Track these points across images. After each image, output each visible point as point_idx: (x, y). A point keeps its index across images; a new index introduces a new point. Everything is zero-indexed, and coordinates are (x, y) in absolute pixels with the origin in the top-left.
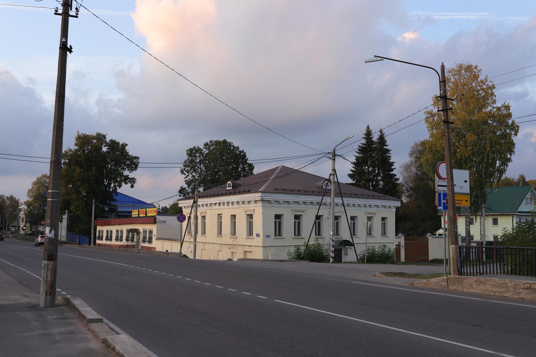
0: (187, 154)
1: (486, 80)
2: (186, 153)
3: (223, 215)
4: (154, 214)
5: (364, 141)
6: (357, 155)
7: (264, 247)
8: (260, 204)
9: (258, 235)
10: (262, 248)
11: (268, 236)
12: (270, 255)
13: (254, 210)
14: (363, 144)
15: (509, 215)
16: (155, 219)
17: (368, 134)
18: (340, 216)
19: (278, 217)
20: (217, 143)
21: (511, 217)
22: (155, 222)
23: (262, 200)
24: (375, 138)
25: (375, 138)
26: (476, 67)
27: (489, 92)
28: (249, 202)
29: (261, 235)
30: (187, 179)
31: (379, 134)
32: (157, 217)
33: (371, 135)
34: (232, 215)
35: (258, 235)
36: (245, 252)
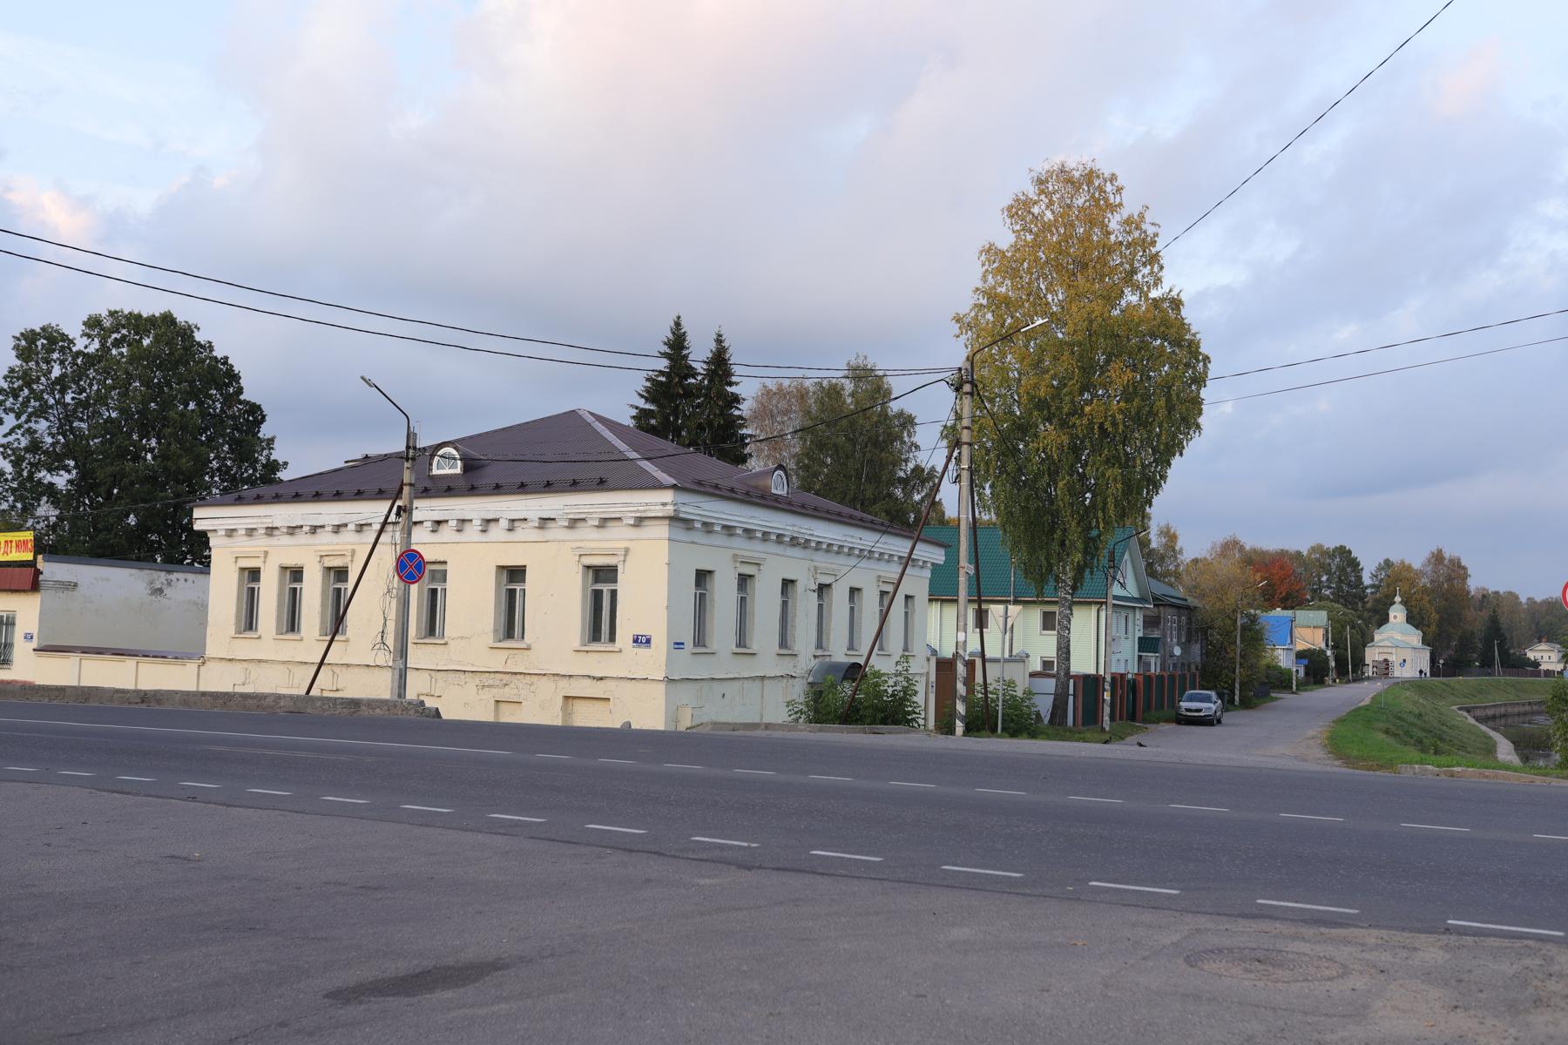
0: (16, 347)
1: (1142, 216)
2: (12, 343)
3: (449, 568)
4: (29, 556)
5: (663, 364)
6: (642, 403)
7: (669, 681)
8: (662, 530)
9: (642, 641)
10: (662, 687)
11: (679, 645)
12: (689, 712)
13: (627, 550)
14: (662, 373)
15: (1090, 603)
16: (38, 573)
17: (677, 344)
18: (829, 586)
19: (702, 576)
20: (138, 323)
21: (1094, 609)
22: (35, 587)
23: (674, 519)
24: (699, 355)
25: (699, 355)
26: (1113, 178)
27: (1144, 249)
28: (250, 532)
29: (660, 642)
30: (10, 439)
31: (713, 346)
32: (41, 564)
33: (683, 348)
34: (501, 568)
35: (642, 641)
36: (566, 698)
